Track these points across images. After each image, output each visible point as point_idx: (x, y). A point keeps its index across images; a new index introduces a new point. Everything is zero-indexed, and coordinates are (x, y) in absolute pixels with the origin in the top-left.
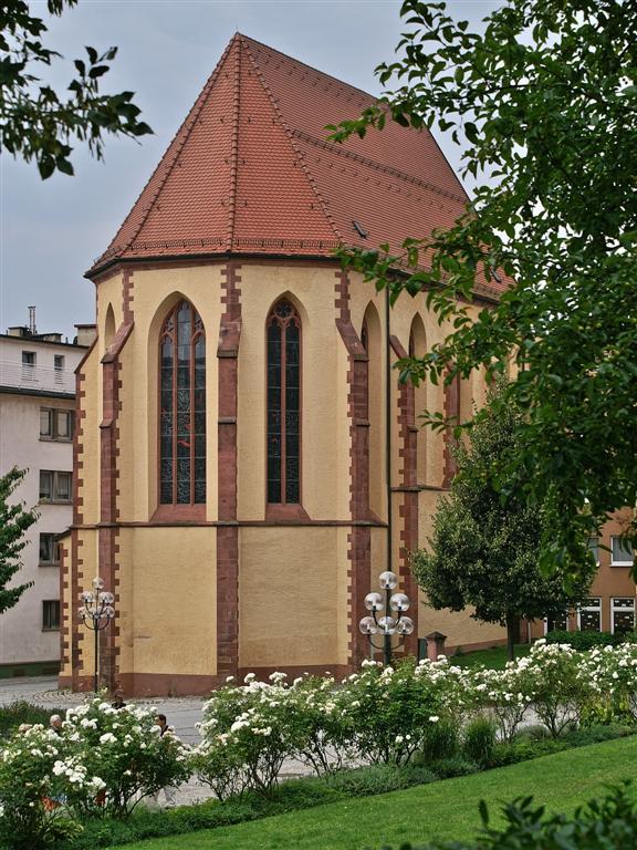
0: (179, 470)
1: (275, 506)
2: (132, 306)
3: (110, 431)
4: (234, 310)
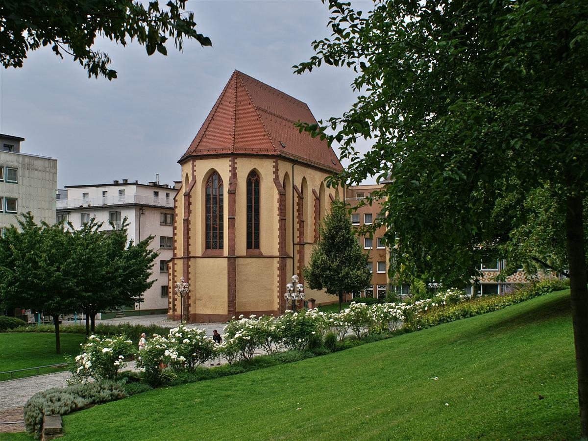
0: (213, 236)
1: (250, 250)
2: (195, 174)
3: (187, 222)
4: (234, 175)
